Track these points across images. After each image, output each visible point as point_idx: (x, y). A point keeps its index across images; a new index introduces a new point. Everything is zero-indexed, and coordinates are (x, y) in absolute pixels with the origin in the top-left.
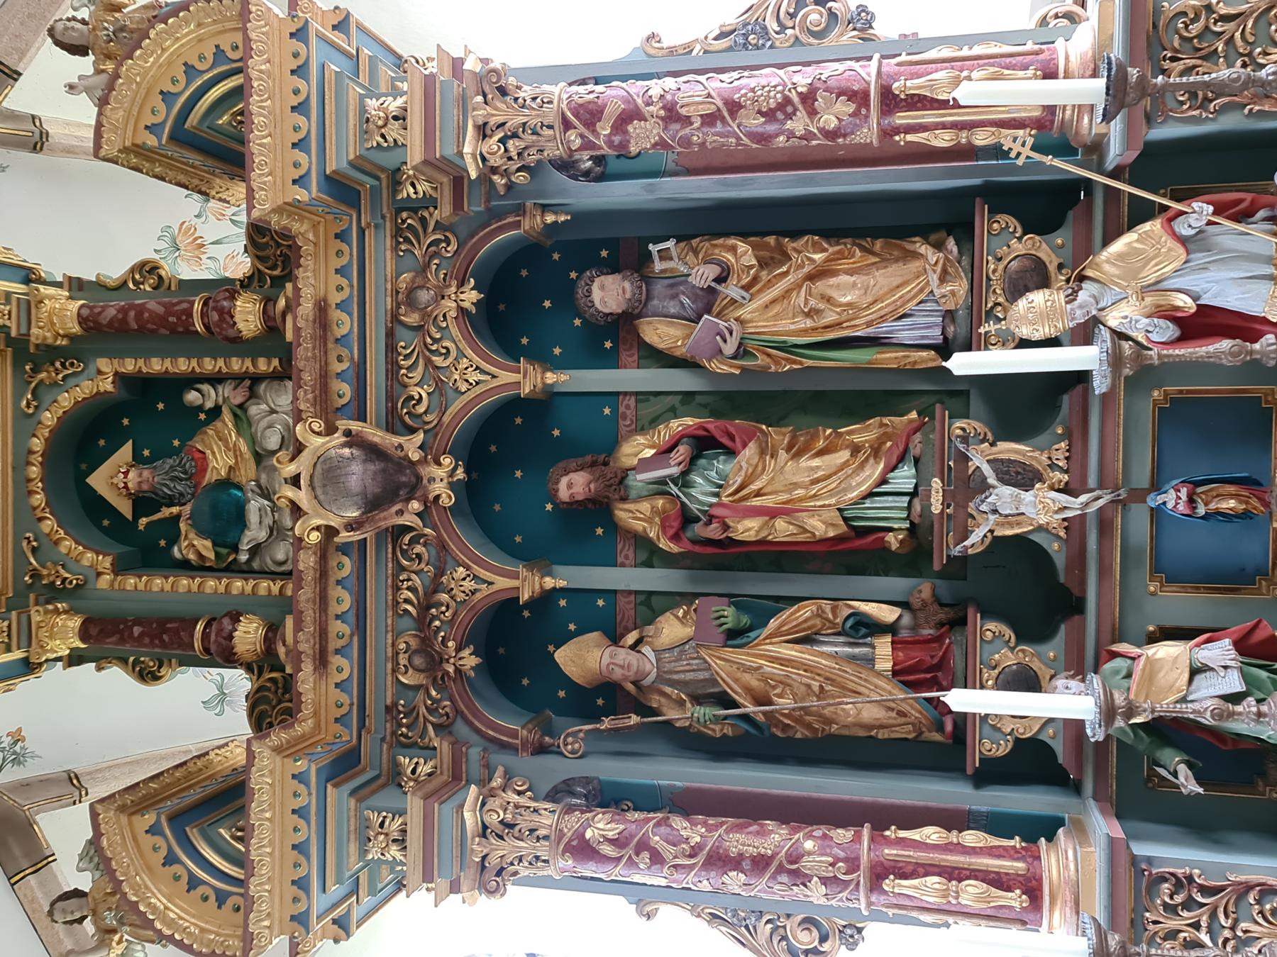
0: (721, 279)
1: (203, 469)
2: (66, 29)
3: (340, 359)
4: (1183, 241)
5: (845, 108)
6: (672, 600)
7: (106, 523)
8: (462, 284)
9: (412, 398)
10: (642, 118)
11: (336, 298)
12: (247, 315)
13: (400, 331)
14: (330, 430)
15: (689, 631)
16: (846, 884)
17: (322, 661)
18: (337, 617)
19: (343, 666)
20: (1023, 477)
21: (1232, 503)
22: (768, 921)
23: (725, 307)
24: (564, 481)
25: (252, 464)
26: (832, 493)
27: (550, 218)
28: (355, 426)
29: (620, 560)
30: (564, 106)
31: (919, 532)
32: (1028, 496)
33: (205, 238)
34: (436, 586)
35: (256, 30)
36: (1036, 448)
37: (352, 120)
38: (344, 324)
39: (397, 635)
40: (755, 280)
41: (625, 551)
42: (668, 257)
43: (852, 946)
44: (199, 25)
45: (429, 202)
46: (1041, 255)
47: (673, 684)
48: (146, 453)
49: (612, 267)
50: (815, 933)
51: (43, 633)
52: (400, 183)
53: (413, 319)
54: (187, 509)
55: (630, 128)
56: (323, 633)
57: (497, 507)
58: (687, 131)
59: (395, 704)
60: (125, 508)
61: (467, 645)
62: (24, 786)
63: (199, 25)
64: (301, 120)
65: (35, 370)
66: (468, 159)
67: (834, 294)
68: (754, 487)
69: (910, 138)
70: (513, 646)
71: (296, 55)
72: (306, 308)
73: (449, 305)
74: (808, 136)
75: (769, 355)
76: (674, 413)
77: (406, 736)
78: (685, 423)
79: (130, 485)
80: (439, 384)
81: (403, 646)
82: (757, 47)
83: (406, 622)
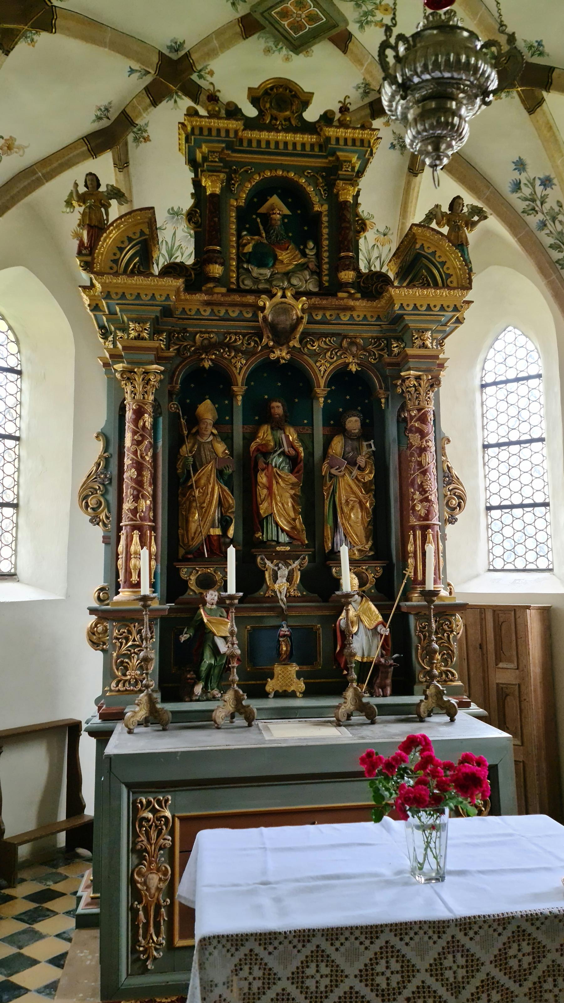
0: (360, 468)
1: (281, 249)
2: (460, 204)
3: (331, 315)
4: (376, 628)
5: (423, 513)
6: (230, 447)
8: (358, 364)
9: (314, 343)
11: (355, 314)
12: (347, 276)
13: (341, 338)
14: (303, 310)
15: (221, 455)
16: (135, 516)
17: (208, 303)
18: (227, 311)
19: (206, 312)
20: (290, 579)
21: (284, 649)
22: (99, 487)
23: (349, 470)
24: (279, 404)
25: (284, 270)
26: (278, 511)
27: (383, 400)
29: (245, 426)
30: (426, 409)
31: (263, 545)
32: (284, 580)
33: (375, 251)
34: (237, 350)
35: (458, 293)
36: (298, 585)
37: (423, 326)
38: (345, 317)
39: (216, 333)
40: (359, 481)
42: (367, 448)
43: (91, 521)
44: (460, 269)
45: (390, 353)
46: (368, 585)
47: (199, 448)
48: (286, 220)
49: (363, 424)
50: (95, 506)
51: (214, 178)
52: (398, 341)
53: (345, 344)
55: (417, 434)
56: (221, 304)
58: (416, 455)
59: (187, 332)
60: (262, 210)
61: (213, 363)
62: (126, 144)
63: (460, 269)
64: (424, 308)
65: (322, 177)
66: (408, 372)
67: (354, 511)
69: (412, 536)
70: (215, 383)
71: (448, 307)
72: (352, 303)
74: (413, 500)
75: (330, 486)
77: (174, 336)
79: (274, 216)
80: (318, 354)
81: (212, 336)
82: (444, 481)
83: (222, 337)
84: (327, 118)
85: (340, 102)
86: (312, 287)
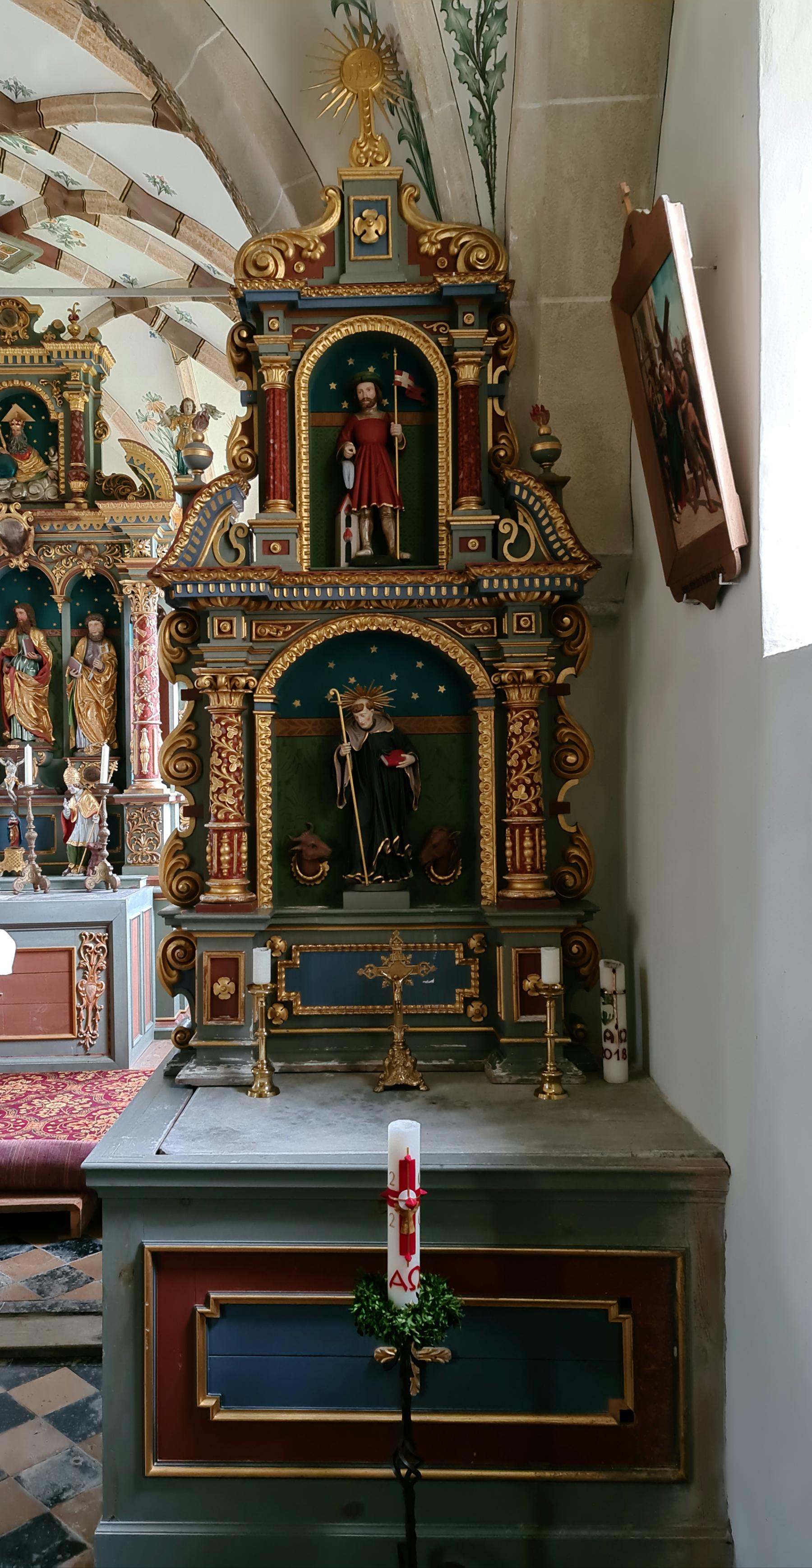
3: (58, 526)
10: (140, 644)
13: (75, 546)
14: (30, 524)
27: (120, 604)
28: (33, 532)
32: (13, 775)
38: (71, 527)
65: (57, 385)
68: (22, 684)
73: (85, 565)
76: (54, 651)
78: (49, 654)
80: (56, 561)
84: (56, 330)
85: (69, 310)
86: (50, 495)
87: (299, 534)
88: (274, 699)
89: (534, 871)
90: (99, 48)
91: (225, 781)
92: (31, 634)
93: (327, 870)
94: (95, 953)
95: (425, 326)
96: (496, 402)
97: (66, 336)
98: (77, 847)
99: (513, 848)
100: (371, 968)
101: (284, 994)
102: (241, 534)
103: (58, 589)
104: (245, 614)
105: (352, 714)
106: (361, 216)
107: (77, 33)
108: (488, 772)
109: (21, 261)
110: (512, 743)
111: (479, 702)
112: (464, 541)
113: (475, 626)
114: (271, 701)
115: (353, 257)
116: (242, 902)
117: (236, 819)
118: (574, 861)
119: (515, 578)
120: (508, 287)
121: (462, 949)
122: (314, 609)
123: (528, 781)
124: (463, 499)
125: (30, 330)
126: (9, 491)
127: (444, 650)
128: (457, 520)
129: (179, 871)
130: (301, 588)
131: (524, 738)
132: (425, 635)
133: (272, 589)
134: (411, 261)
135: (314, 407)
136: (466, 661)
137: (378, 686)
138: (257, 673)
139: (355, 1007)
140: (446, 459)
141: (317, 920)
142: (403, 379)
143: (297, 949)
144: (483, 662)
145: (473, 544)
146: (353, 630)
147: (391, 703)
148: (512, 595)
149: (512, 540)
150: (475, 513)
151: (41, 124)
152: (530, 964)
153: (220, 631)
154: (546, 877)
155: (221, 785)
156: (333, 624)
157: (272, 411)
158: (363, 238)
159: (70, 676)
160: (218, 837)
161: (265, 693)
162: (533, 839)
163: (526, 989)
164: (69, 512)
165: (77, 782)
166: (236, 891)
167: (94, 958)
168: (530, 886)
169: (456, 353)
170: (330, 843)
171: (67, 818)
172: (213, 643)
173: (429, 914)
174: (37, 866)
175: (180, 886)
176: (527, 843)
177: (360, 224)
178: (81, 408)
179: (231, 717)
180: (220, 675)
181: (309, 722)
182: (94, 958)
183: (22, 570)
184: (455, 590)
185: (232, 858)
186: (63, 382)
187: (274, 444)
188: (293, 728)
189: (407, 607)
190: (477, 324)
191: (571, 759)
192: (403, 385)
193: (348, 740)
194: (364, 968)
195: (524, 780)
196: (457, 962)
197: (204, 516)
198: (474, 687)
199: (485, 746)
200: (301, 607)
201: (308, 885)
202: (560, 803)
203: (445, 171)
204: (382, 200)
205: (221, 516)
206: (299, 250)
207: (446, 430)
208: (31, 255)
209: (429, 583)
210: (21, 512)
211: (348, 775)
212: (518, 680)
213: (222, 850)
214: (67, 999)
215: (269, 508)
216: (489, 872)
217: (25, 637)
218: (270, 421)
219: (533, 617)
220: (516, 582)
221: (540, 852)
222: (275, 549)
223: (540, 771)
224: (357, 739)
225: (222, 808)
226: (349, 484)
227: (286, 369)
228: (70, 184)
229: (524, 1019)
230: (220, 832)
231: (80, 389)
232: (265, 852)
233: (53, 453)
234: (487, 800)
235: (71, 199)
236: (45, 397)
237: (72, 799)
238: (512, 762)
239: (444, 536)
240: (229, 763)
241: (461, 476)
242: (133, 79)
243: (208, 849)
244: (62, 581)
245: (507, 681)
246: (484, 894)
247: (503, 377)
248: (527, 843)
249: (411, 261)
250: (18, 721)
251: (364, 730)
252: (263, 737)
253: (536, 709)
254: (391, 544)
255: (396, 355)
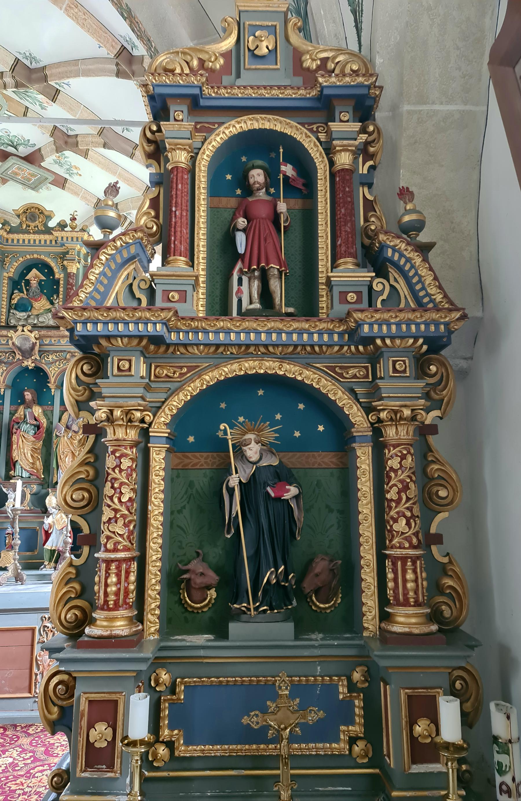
3: (55, 341)
7: (25, 271)
13: (66, 353)
14: (36, 339)
24: (29, 393)
41: (14, 408)
54: (25, 296)
57: (27, 375)
65: (61, 258)
68: (24, 440)
78: (44, 421)
80: (52, 363)
84: (62, 226)
85: (71, 215)
87: (195, 286)
88: (169, 433)
89: (417, 604)
90: (79, 19)
91: (116, 511)
92: (33, 408)
93: (214, 597)
94: (52, 631)
95: (306, 126)
96: (366, 190)
97: (68, 229)
98: (51, 550)
99: (395, 580)
100: (257, 716)
101: (167, 732)
102: (143, 286)
103: (52, 380)
104: (143, 354)
105: (241, 449)
106: (254, 36)
107: (64, 6)
108: (367, 504)
109: (40, 183)
110: (391, 477)
111: (357, 439)
112: (343, 295)
113: (352, 372)
114: (167, 435)
115: (247, 66)
116: (125, 636)
117: (126, 549)
118: (448, 591)
119: (394, 323)
120: (377, 93)
121: (345, 683)
122: (208, 354)
123: (408, 514)
124: (341, 261)
125: (45, 225)
126: (26, 320)
127: (324, 391)
128: (337, 276)
129: (70, 599)
130: (196, 331)
131: (403, 472)
132: (308, 378)
133: (170, 332)
134: (295, 74)
135: (214, 191)
136: (344, 402)
137: (265, 423)
138: (154, 409)
139: (239, 747)
140: (325, 230)
141: (202, 653)
142: (288, 169)
143: (181, 683)
144: (360, 403)
145: (351, 297)
146: (242, 373)
147: (276, 439)
148: (388, 341)
149: (384, 297)
150: (353, 271)
151: (46, 81)
152: (425, 708)
153: (119, 368)
154: (429, 611)
155: (112, 515)
156: (225, 366)
157: (175, 185)
158: (255, 52)
159: (56, 435)
160: (106, 567)
161: (160, 427)
162: (415, 571)
163: (416, 735)
164: (62, 332)
165: (54, 505)
166: (122, 623)
167: (50, 635)
168: (413, 620)
169: (334, 142)
170: (217, 570)
171: (46, 530)
172: (112, 379)
173: (313, 647)
174: (18, 565)
175: (69, 616)
176: (410, 576)
177: (253, 41)
178: (75, 271)
179: (126, 449)
180: (116, 409)
181: (202, 456)
182: (50, 635)
183: (30, 368)
184: (336, 337)
185: (119, 589)
186: (64, 256)
187: (175, 212)
188: (187, 461)
189: (292, 353)
190: (352, 119)
191: (443, 493)
192: (287, 174)
193: (237, 472)
194: (249, 716)
195: (404, 513)
196: (341, 697)
197: (110, 267)
198: (353, 425)
199: (363, 480)
200: (196, 352)
201: (195, 612)
202: (432, 534)
203: (322, 13)
204: (272, 26)
205: (126, 270)
206: (202, 62)
207: (325, 207)
208: (47, 179)
209: (312, 330)
210: (31, 331)
211: (236, 505)
212: (396, 418)
213: (109, 581)
214: (28, 666)
215: (169, 264)
216: (370, 602)
217: (29, 410)
218: (174, 193)
219: (407, 362)
220: (394, 327)
221: (422, 584)
222: (173, 297)
223: (417, 504)
224: (245, 471)
225: (111, 538)
226: (241, 249)
227: (188, 152)
228: (69, 131)
229: (416, 769)
230: (108, 562)
231: (74, 260)
232: (154, 581)
233: (55, 297)
234: (367, 531)
235: (70, 140)
236: (53, 264)
237: (51, 517)
238: (392, 495)
239: (324, 293)
240: (121, 493)
241: (339, 243)
242: (102, 41)
243: (97, 579)
244: (55, 375)
245: (386, 419)
246: (366, 625)
247: (373, 168)
248: (410, 576)
249: (295, 74)
250: (20, 464)
251: (251, 462)
252: (157, 468)
253: (411, 445)
254: (277, 301)
255: (281, 150)
